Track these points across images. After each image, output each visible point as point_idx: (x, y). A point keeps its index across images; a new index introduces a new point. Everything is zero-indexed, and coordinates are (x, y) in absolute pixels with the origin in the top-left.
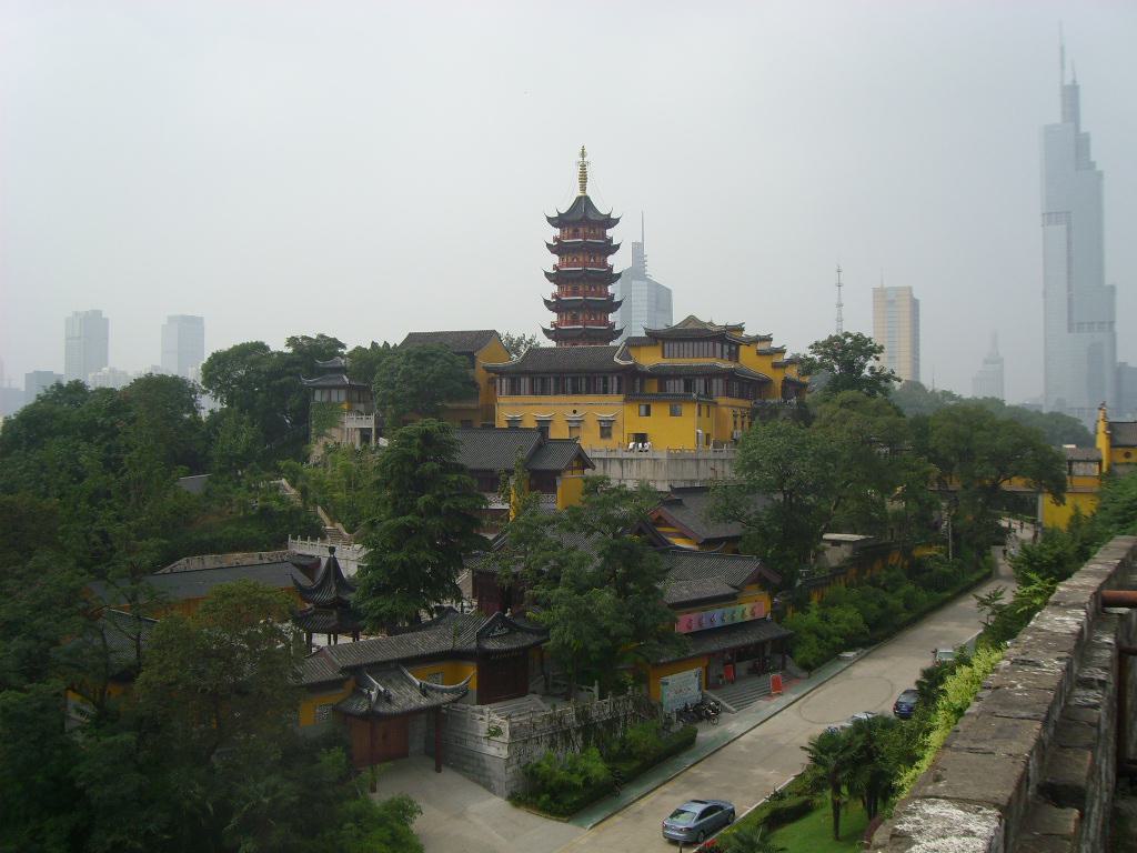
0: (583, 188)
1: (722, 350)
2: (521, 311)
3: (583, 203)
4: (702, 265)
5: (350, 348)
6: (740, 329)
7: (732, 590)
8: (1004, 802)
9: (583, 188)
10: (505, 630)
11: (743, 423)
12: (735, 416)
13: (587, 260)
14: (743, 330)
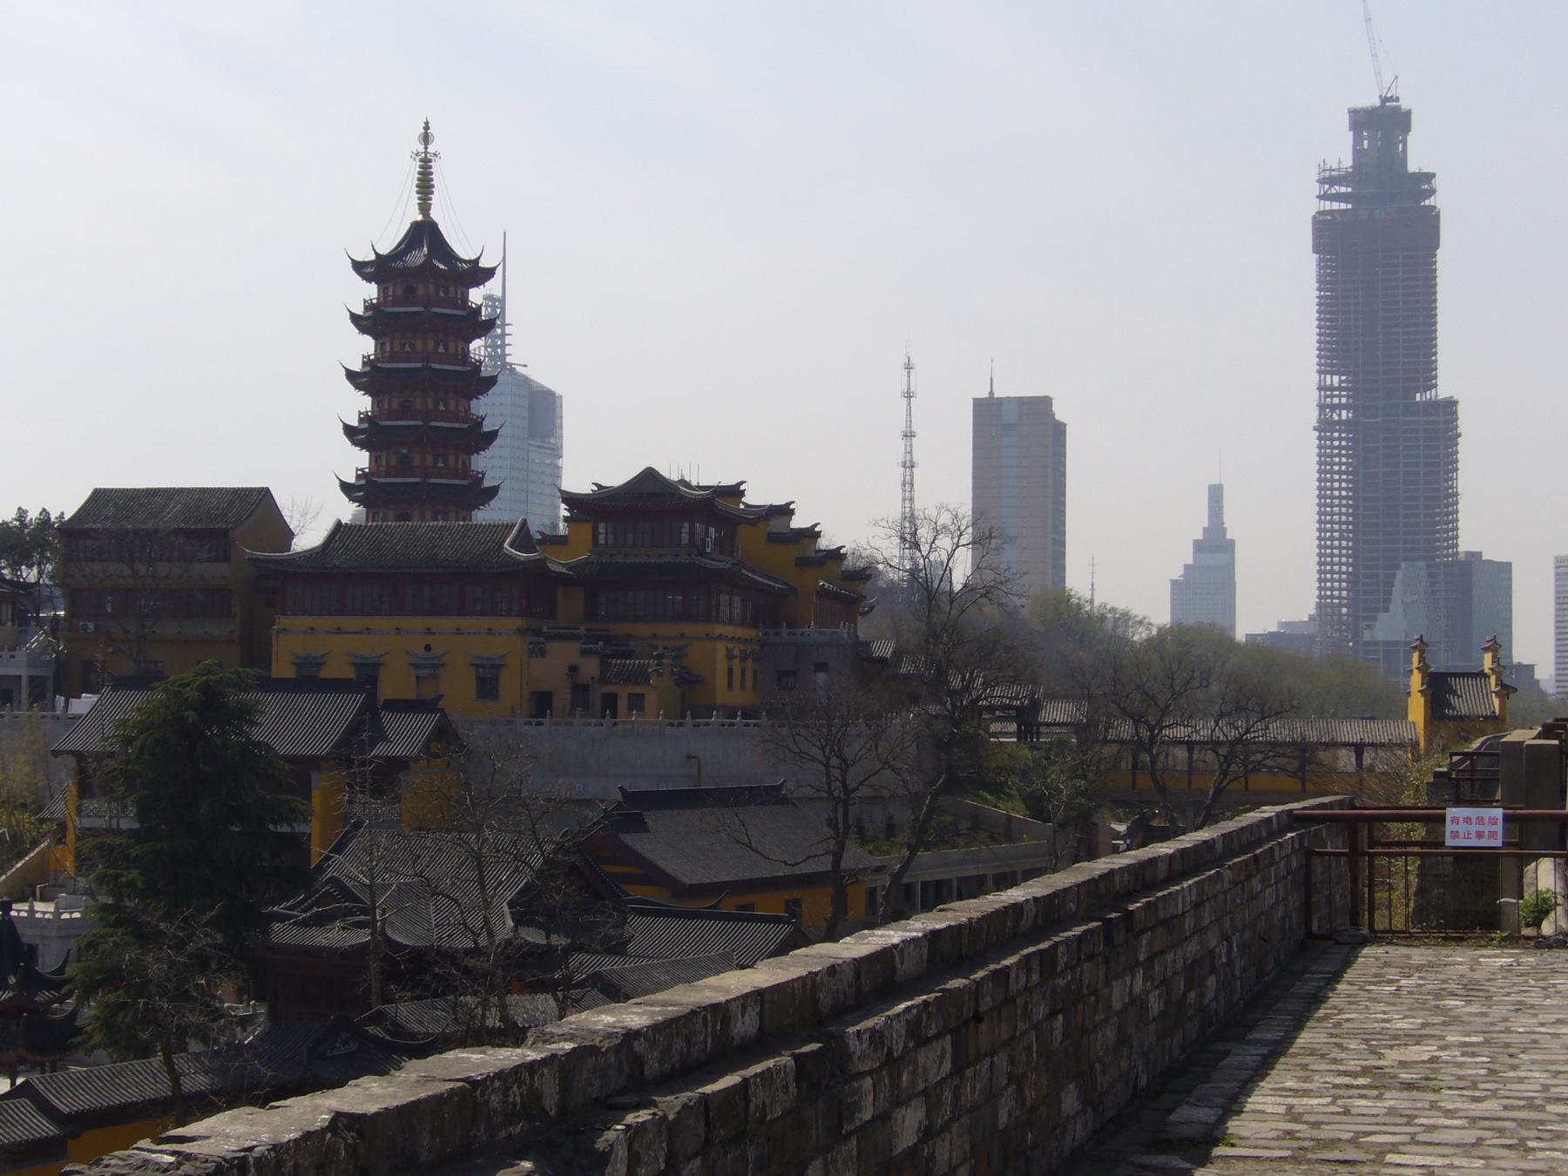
0: (425, 207)
1: (731, 604)
3: (425, 233)
4: (619, 391)
5: (257, 735)
6: (735, 492)
8: (743, 530)
9: (425, 207)
10: (354, 1046)
11: (743, 672)
12: (730, 657)
13: (429, 462)
14: (742, 494)
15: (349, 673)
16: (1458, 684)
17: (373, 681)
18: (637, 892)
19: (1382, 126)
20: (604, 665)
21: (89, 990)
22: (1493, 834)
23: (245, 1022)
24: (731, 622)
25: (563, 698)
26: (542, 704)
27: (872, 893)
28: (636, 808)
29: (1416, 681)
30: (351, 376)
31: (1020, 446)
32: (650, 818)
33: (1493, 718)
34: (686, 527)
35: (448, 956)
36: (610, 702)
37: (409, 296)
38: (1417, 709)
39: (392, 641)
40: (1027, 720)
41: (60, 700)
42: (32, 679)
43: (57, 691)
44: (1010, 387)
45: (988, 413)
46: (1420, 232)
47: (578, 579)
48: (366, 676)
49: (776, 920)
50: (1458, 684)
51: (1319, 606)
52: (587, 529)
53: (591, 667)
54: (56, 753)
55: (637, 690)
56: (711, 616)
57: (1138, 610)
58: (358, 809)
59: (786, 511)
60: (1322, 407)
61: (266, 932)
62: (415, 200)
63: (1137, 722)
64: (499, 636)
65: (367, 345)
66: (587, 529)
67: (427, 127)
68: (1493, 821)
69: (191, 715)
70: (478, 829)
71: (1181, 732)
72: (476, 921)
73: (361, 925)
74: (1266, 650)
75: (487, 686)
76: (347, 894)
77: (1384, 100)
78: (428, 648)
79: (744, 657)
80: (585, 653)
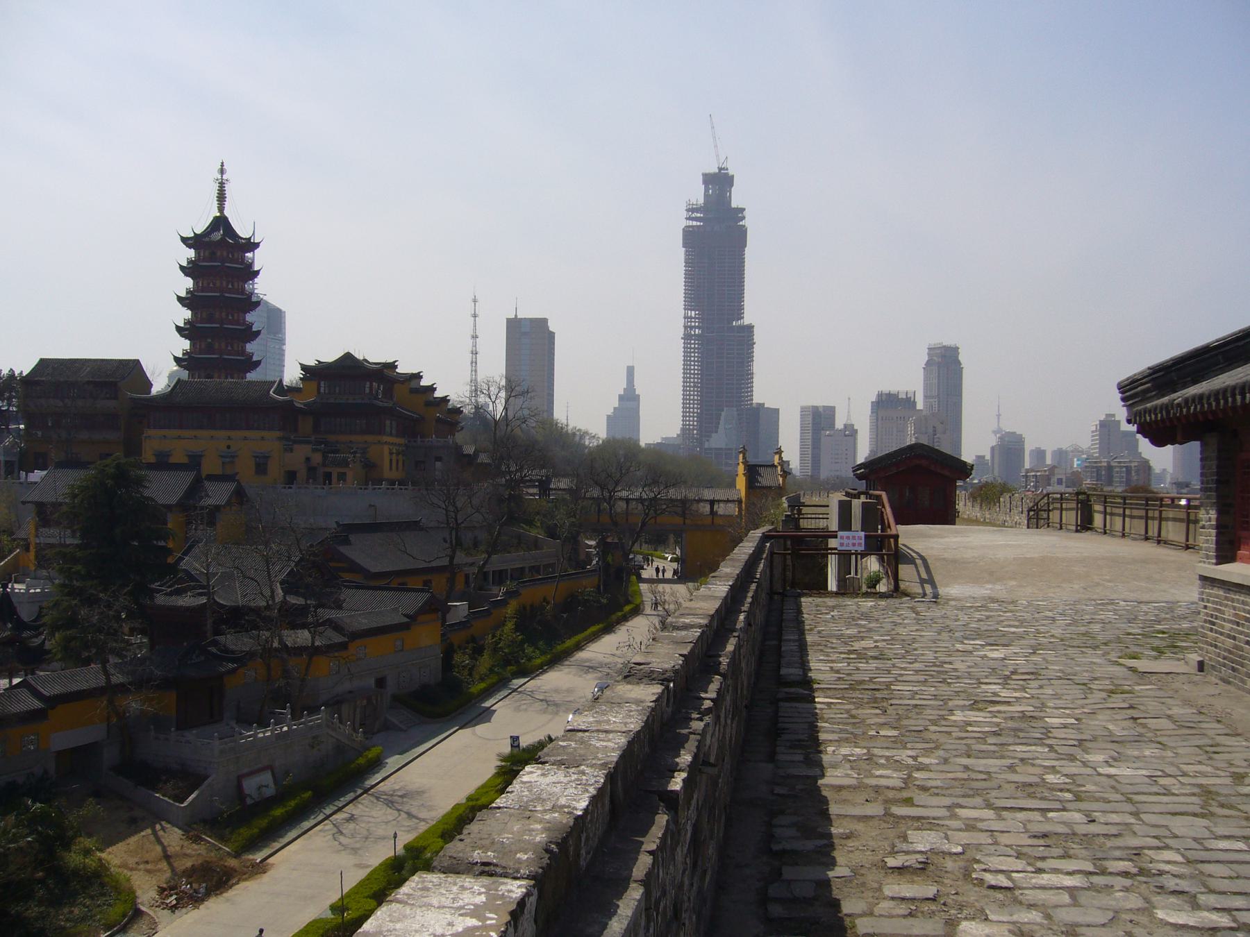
0: (221, 209)
2: (155, 344)
3: (221, 223)
5: (147, 493)
6: (393, 366)
7: (406, 620)
9: (221, 209)
12: (391, 454)
15: (185, 460)
16: (761, 470)
17: (199, 465)
18: (347, 576)
19: (719, 182)
20: (325, 457)
21: (55, 628)
22: (860, 544)
23: (140, 646)
24: (391, 434)
25: (302, 474)
26: (291, 477)
27: (467, 576)
28: (348, 531)
29: (741, 469)
30: (180, 299)
31: (531, 343)
32: (352, 538)
33: (779, 488)
34: (368, 384)
35: (257, 611)
36: (328, 477)
37: (212, 257)
38: (741, 483)
39: (210, 443)
40: (544, 487)
41: (23, 474)
42: (7, 462)
43: (21, 469)
44: (528, 312)
45: (515, 326)
46: (738, 238)
47: (310, 411)
48: (194, 462)
49: (422, 591)
50: (761, 470)
51: (683, 429)
52: (313, 385)
53: (317, 458)
54: (24, 503)
55: (342, 470)
56: (381, 432)
57: (593, 431)
58: (199, 532)
59: (418, 376)
60: (686, 327)
61: (152, 598)
62: (216, 204)
63: (602, 489)
64: (267, 441)
65: (189, 283)
66: (313, 385)
67: (222, 165)
68: (860, 538)
69: (110, 482)
70: (266, 544)
71: (624, 494)
72: (267, 593)
73: (201, 594)
74: (657, 451)
75: (261, 467)
76: (191, 578)
77: (720, 169)
78: (229, 447)
79: (398, 454)
80: (314, 450)
